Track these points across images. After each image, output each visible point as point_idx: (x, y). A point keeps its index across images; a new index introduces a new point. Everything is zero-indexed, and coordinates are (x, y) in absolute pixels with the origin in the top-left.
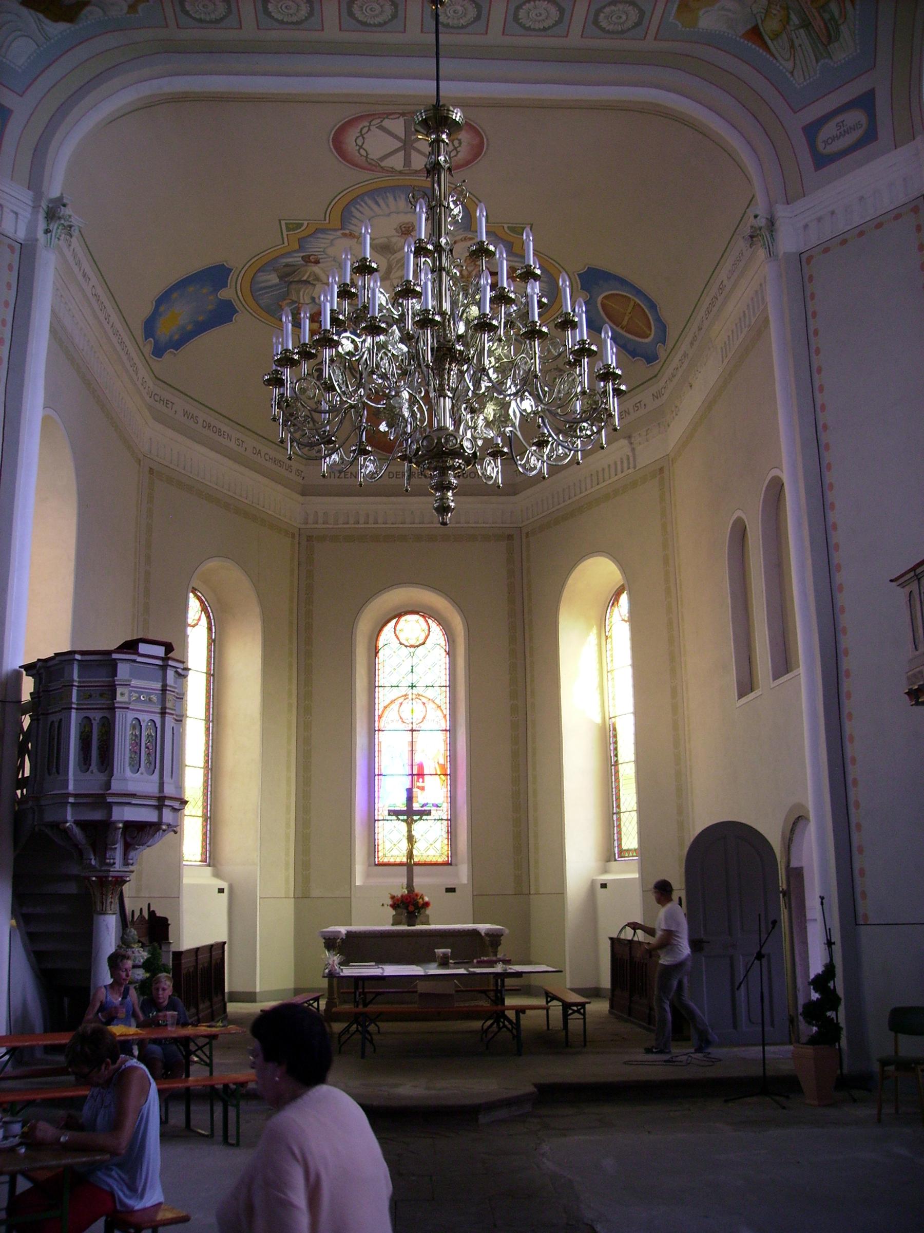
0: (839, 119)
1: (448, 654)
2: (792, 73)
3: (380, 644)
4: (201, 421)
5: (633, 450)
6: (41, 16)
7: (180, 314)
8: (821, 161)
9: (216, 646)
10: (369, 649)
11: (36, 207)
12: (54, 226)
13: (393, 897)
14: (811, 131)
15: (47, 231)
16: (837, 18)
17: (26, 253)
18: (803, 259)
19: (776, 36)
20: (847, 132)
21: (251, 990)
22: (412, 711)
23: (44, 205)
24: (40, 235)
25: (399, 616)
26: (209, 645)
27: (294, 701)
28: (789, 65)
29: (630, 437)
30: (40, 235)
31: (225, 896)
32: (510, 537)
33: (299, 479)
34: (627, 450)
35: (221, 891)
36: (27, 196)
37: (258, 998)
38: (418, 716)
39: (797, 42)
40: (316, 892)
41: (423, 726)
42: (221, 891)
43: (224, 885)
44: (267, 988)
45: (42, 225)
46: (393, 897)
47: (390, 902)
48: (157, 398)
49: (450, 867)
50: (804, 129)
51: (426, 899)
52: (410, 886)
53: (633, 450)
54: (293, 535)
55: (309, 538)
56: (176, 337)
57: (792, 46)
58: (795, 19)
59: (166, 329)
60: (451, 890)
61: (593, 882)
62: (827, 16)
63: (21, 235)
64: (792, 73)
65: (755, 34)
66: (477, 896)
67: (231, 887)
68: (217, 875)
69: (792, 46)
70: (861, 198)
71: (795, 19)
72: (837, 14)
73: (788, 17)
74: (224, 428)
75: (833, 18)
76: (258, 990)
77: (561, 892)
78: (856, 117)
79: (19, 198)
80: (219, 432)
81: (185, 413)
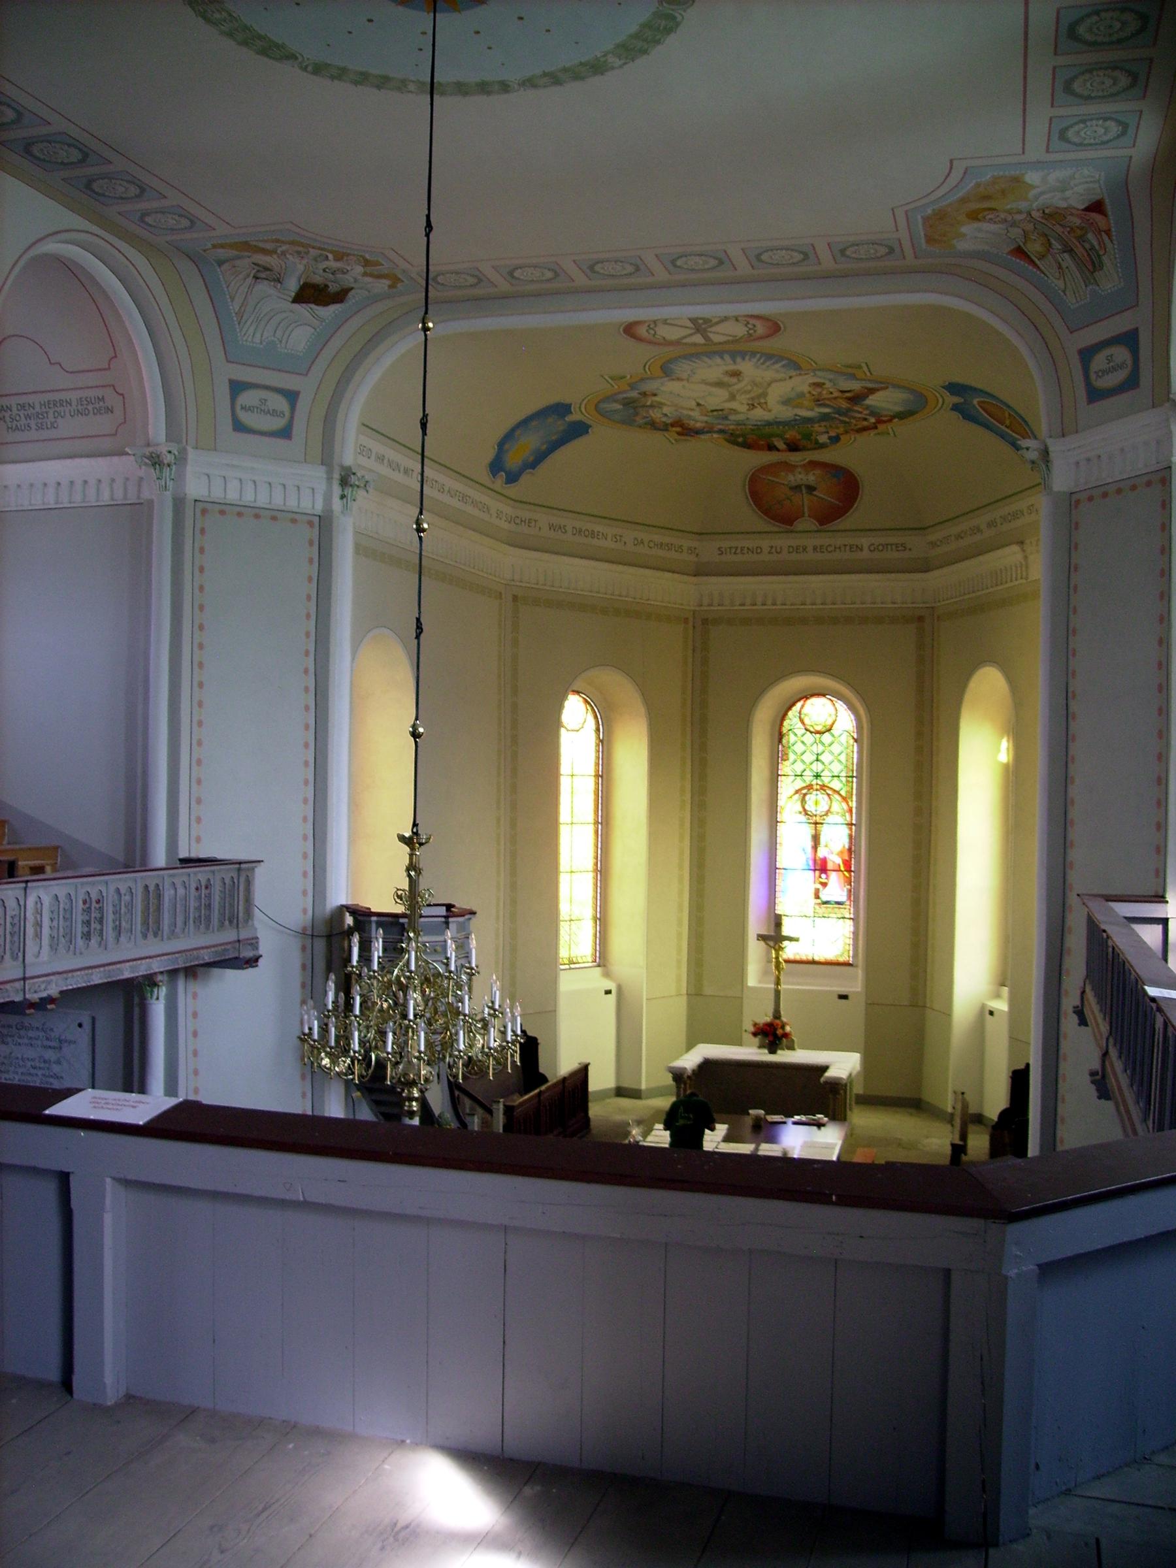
0: (1107, 352)
1: (856, 740)
2: (1064, 291)
3: (784, 730)
4: (569, 529)
5: (1026, 558)
6: (313, 306)
7: (530, 442)
8: (1095, 395)
9: (605, 745)
10: (772, 735)
11: (329, 479)
12: (348, 491)
13: (755, 1025)
14: (1086, 355)
15: (343, 497)
16: (1097, 247)
17: (324, 525)
18: (1071, 503)
19: (1042, 257)
20: (1114, 369)
21: (634, 1086)
22: (817, 802)
23: (336, 476)
24: (337, 504)
25: (806, 698)
26: (598, 745)
27: (688, 796)
28: (1061, 284)
29: (1022, 543)
30: (337, 504)
31: (612, 998)
32: (920, 619)
33: (693, 558)
34: (1019, 557)
35: (608, 992)
36: (320, 472)
37: (643, 1095)
38: (823, 807)
39: (1064, 265)
40: (708, 991)
41: (828, 819)
42: (608, 992)
43: (611, 985)
44: (653, 1085)
45: (337, 490)
46: (755, 1025)
47: (752, 1029)
48: (518, 521)
49: (850, 968)
50: (1081, 352)
51: (788, 1029)
52: (777, 1015)
53: (1026, 558)
54: (686, 620)
55: (705, 621)
56: (531, 459)
57: (1060, 267)
58: (1057, 245)
59: (513, 460)
60: (843, 997)
61: (983, 1006)
62: (1087, 246)
63: (319, 507)
64: (1064, 291)
65: (1019, 252)
66: (871, 1005)
67: (620, 988)
68: (607, 975)
69: (1060, 267)
70: (1122, 450)
71: (1057, 245)
72: (1095, 243)
73: (1050, 244)
74: (598, 528)
75: (1093, 248)
76: (643, 1087)
77: (947, 1013)
78: (1121, 354)
79: (316, 476)
80: (593, 534)
81: (551, 527)
